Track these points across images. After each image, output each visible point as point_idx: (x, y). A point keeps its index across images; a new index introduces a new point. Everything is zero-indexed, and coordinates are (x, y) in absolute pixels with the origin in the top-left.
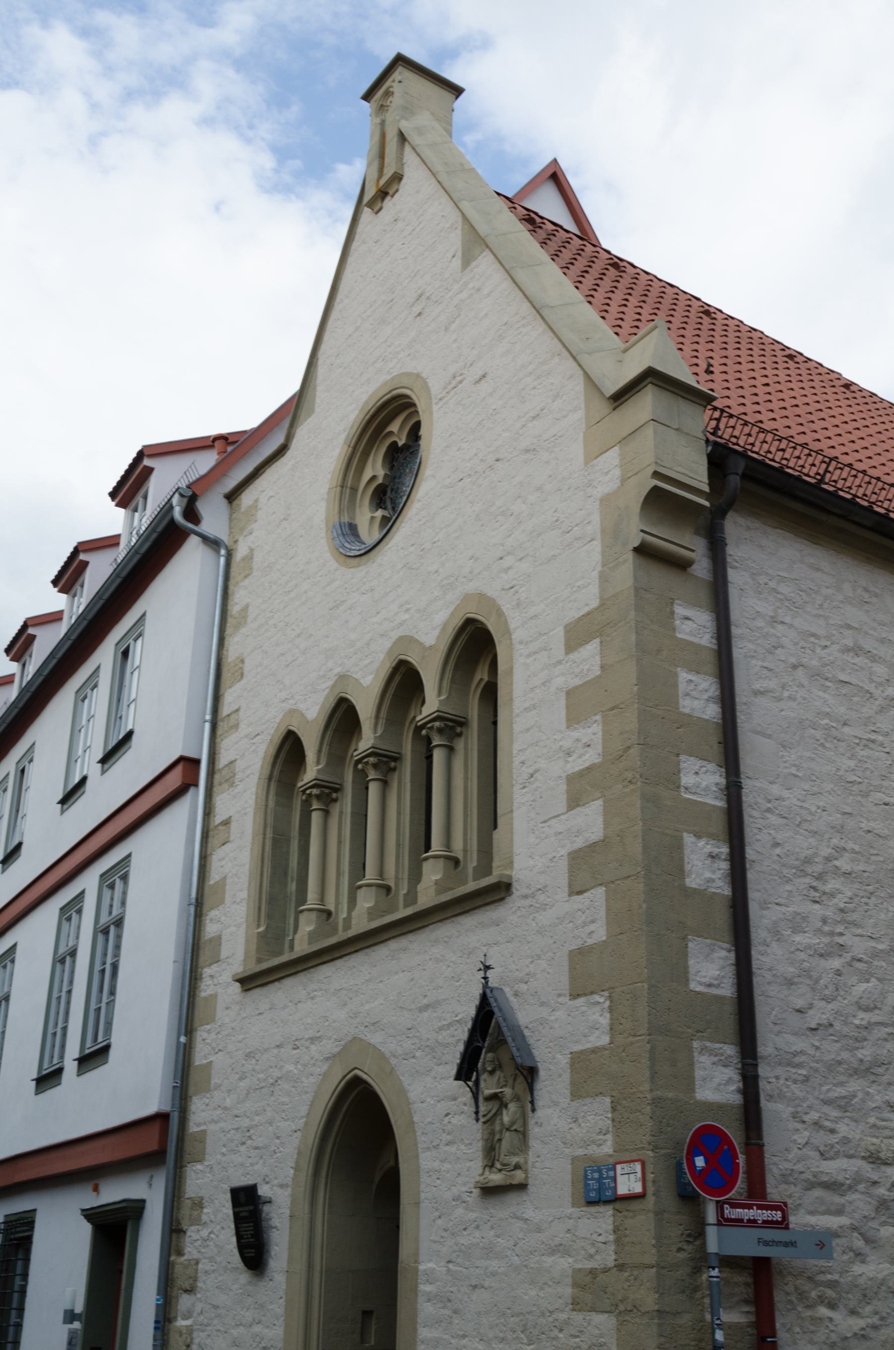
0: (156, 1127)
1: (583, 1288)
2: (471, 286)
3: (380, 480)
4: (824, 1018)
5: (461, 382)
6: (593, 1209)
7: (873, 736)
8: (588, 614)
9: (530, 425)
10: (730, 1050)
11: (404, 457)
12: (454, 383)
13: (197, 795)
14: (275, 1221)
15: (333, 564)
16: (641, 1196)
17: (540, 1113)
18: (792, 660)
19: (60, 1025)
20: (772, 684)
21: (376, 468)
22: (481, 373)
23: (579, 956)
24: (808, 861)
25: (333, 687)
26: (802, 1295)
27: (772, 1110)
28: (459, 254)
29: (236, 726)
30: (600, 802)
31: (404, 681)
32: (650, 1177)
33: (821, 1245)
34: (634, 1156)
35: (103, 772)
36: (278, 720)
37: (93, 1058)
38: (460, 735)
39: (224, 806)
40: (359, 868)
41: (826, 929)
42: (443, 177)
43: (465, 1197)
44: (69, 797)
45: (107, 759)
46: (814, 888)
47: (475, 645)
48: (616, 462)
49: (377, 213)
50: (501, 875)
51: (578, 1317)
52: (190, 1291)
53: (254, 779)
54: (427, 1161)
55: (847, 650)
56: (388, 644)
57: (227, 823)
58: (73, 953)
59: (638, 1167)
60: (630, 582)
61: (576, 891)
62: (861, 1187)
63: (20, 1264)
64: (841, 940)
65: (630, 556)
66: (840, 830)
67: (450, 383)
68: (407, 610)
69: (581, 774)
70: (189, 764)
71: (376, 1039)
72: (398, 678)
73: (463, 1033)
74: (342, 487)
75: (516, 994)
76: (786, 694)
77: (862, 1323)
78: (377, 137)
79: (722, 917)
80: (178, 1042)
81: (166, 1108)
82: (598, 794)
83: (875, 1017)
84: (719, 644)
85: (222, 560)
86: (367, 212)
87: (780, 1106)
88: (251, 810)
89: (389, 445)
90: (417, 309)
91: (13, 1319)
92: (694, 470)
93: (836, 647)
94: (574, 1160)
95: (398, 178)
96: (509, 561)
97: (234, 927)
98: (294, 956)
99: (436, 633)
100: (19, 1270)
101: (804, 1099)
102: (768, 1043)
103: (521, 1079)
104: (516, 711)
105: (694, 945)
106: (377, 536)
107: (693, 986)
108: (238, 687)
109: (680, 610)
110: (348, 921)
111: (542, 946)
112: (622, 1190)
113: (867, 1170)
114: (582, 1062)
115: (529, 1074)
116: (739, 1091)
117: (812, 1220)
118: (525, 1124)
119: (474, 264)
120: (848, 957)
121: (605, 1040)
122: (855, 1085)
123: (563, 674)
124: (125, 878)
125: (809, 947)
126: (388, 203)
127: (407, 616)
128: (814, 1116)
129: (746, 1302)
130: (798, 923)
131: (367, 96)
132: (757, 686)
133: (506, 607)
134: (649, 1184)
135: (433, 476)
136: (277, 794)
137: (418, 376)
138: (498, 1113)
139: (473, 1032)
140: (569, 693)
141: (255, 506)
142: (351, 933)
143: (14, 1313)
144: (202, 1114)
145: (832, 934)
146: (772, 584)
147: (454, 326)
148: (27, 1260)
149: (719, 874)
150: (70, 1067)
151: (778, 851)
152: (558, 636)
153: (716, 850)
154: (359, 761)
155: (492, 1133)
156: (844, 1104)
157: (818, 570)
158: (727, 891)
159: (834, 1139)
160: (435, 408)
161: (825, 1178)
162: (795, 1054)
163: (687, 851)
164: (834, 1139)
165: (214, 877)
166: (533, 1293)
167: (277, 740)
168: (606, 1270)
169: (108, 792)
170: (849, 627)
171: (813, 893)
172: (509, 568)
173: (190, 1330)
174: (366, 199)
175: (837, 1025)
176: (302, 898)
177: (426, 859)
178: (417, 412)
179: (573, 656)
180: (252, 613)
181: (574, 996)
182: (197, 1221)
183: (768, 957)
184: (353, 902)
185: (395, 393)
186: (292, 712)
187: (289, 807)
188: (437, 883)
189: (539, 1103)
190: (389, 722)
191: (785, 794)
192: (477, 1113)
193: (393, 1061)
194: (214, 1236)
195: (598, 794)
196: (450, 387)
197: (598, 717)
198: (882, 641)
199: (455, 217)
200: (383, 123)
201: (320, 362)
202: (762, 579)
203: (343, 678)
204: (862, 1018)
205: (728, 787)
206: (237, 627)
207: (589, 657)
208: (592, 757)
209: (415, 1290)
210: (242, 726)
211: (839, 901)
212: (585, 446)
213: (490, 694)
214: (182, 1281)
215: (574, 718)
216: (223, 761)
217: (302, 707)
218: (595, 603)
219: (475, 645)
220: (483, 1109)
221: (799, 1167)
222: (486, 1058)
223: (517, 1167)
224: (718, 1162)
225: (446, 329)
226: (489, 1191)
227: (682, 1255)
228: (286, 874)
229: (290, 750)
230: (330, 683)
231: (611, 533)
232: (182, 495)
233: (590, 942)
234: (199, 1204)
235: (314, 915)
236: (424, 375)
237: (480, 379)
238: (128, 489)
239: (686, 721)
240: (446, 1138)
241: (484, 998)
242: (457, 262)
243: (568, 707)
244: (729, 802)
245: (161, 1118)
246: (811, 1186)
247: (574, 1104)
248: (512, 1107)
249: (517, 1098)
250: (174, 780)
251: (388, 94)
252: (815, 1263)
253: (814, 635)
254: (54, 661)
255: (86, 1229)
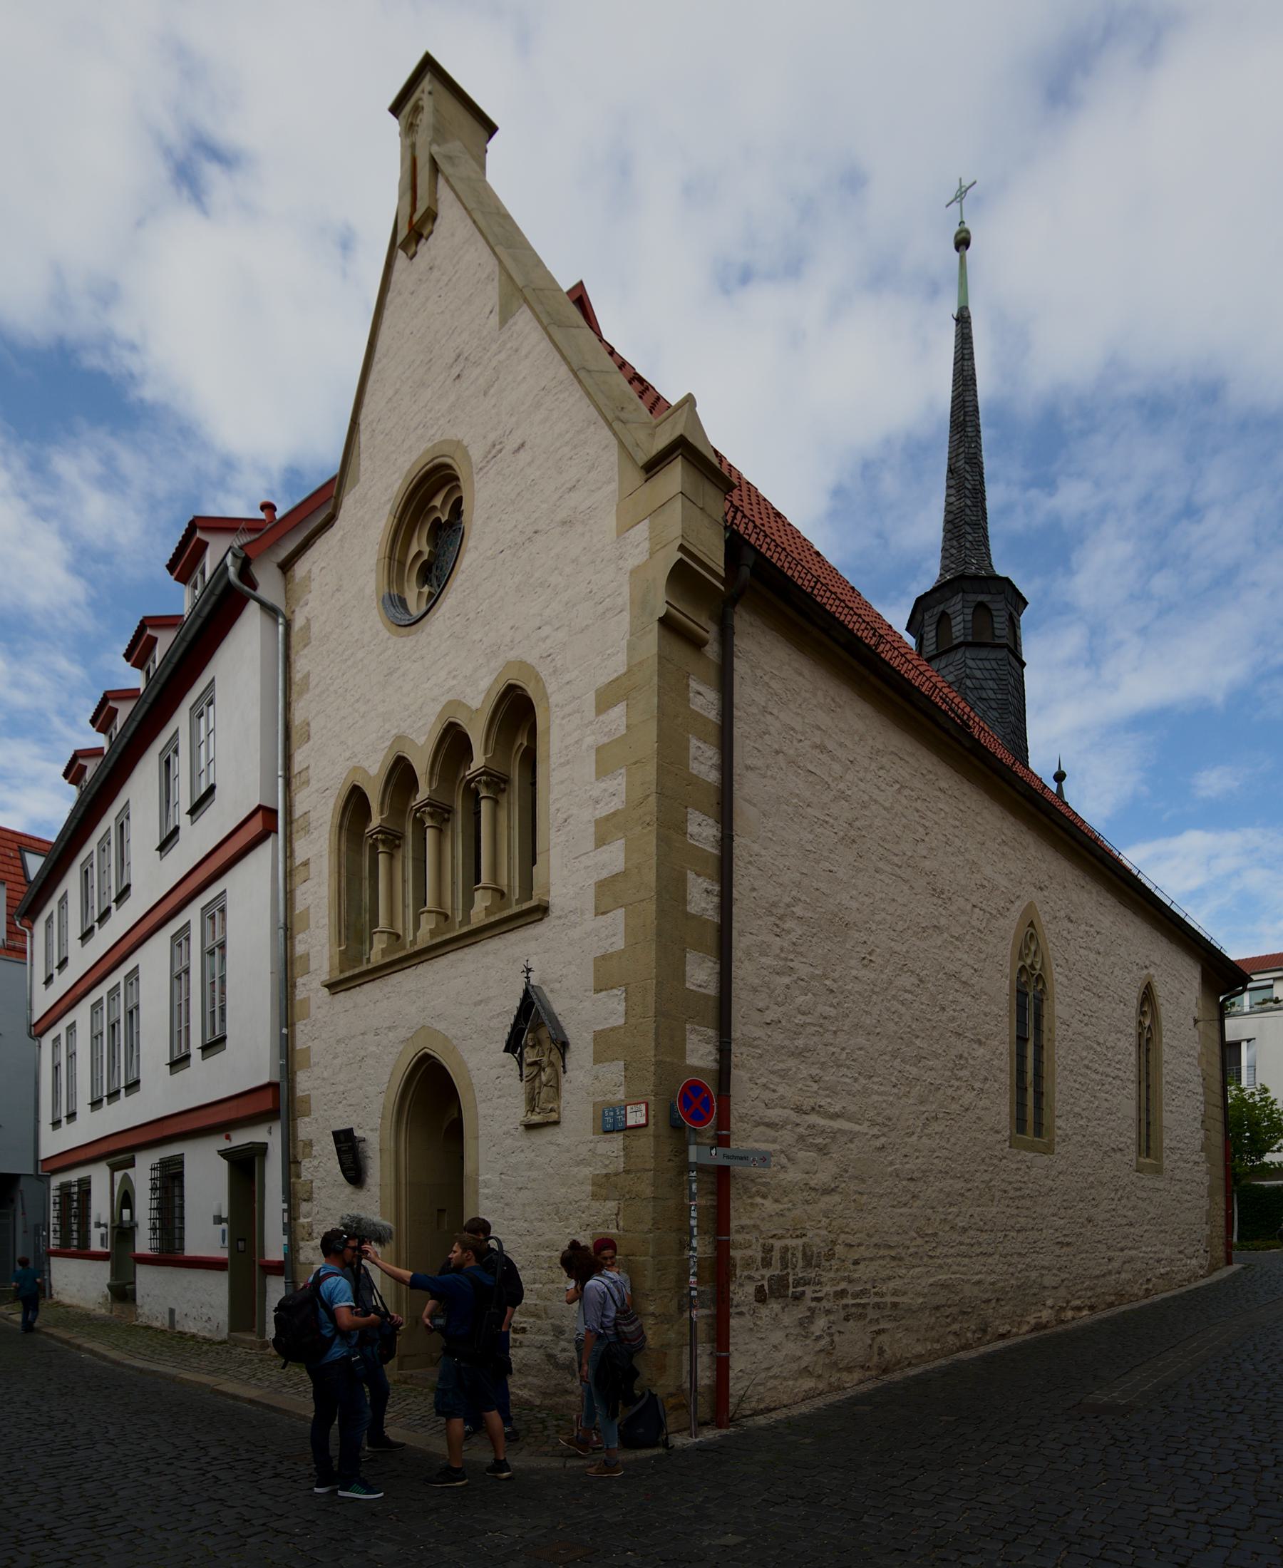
0: (270, 1092)
1: (600, 1186)
2: (509, 345)
3: (425, 557)
4: (775, 1017)
5: (500, 451)
6: (608, 1136)
7: (827, 819)
8: (617, 679)
9: (566, 496)
10: (711, 1033)
11: (448, 534)
12: (494, 452)
13: (277, 840)
14: (370, 1154)
15: (385, 633)
16: (646, 1125)
17: (568, 1074)
18: (776, 746)
19: (183, 1025)
20: (759, 763)
21: (420, 544)
22: (519, 441)
23: (602, 961)
24: (774, 904)
25: (391, 747)
26: (746, 1190)
27: (738, 1075)
28: (497, 309)
29: (307, 782)
30: (623, 841)
31: (453, 742)
32: (652, 1113)
33: (764, 1159)
34: (641, 1099)
35: (193, 823)
36: (344, 776)
37: (214, 1045)
38: (504, 790)
39: (303, 849)
40: (421, 900)
41: (783, 955)
42: (477, 216)
43: (513, 1132)
44: (166, 843)
45: (195, 810)
46: (777, 926)
47: (516, 710)
48: (646, 534)
49: (412, 258)
50: (540, 900)
51: (596, 1204)
52: (308, 1200)
53: (327, 827)
54: (483, 1109)
55: (815, 747)
56: (439, 708)
57: (306, 864)
58: (187, 971)
59: (643, 1107)
60: (655, 650)
61: (600, 912)
62: (789, 1127)
63: (177, 1190)
64: (791, 964)
65: (655, 626)
66: (798, 885)
67: (489, 452)
68: (454, 677)
69: (608, 818)
70: (266, 813)
71: (440, 1026)
72: (448, 740)
73: (510, 1020)
74: (390, 558)
75: (552, 991)
76: (769, 773)
77: (781, 1207)
78: (408, 163)
79: (711, 938)
80: (282, 1034)
81: (276, 1079)
82: (621, 835)
83: (808, 1019)
84: (723, 721)
85: (281, 628)
86: (401, 254)
87: (742, 1073)
88: (326, 853)
89: (433, 516)
90: (455, 371)
91: (177, 1224)
92: (714, 553)
93: (807, 742)
94: (595, 1104)
95: (431, 215)
96: (546, 630)
97: (319, 946)
98: (370, 966)
99: (483, 696)
100: (177, 1215)
101: (758, 1069)
102: (739, 1030)
103: (555, 1051)
104: (553, 766)
105: (691, 956)
106: (424, 608)
107: (688, 985)
108: (306, 747)
109: (694, 685)
110: (414, 942)
111: (580, 946)
112: (630, 1122)
113: (794, 1116)
114: (599, 1037)
115: (563, 1046)
116: (716, 1060)
117: (757, 1145)
118: (558, 1082)
119: (511, 322)
120: (795, 976)
121: (622, 1021)
122: (791, 1063)
123: (593, 733)
124: (223, 910)
125: (770, 967)
126: (423, 247)
127: (455, 682)
128: (764, 1080)
129: (712, 1193)
130: (764, 950)
131: (396, 109)
132: (749, 762)
133: (544, 672)
134: (651, 1118)
135: (476, 548)
136: (348, 841)
137: (459, 442)
138: (538, 1074)
139: (517, 1018)
140: (598, 750)
141: (308, 578)
142: (416, 948)
143: (177, 1221)
144: (304, 1083)
145: (786, 959)
146: (766, 678)
147: (492, 391)
148: (182, 1187)
149: (711, 906)
150: (196, 1054)
151: (754, 894)
152: (590, 698)
153: (710, 888)
154: (418, 810)
155: (533, 1088)
156: (783, 1074)
157: (801, 674)
158: (717, 919)
159: (774, 1096)
160: (476, 478)
161: (767, 1120)
162: (755, 1039)
163: (689, 885)
164: (774, 1096)
165: (299, 908)
166: (563, 1190)
167: (345, 793)
168: (617, 1174)
169: (199, 838)
170: (819, 728)
171: (775, 929)
172: (547, 637)
173: (310, 1225)
174: (400, 239)
175: (784, 1023)
176: (374, 921)
177: (477, 889)
178: (458, 487)
179: (603, 717)
180: (313, 680)
181: (597, 991)
182: (310, 1155)
183: (742, 971)
184: (417, 926)
185: (436, 461)
186: (356, 769)
187: (359, 852)
188: (486, 908)
189: (568, 1067)
190: (442, 779)
191: (763, 852)
192: (521, 1075)
193: (455, 1042)
194: (323, 1165)
195: (621, 835)
196: (490, 456)
197: (623, 771)
198: (841, 744)
199: (492, 264)
200: (413, 146)
201: (362, 427)
202: (759, 673)
203: (399, 738)
204: (800, 1019)
205: (722, 839)
206: (301, 694)
207: (617, 716)
208: (617, 804)
209: (476, 1193)
210: (312, 782)
211: (793, 937)
212: (618, 519)
213: (530, 760)
214: (301, 1191)
215: (603, 771)
216: (298, 811)
217: (365, 764)
218: (623, 670)
219: (516, 710)
220: (525, 1072)
221: (751, 1112)
222: (528, 1037)
223: (552, 1110)
224: (698, 1106)
225: (485, 394)
226: (530, 1127)
227: (671, 1164)
228: (360, 907)
229: (355, 801)
230: (388, 743)
231: (640, 604)
232: (234, 555)
233: (611, 950)
234: (309, 1144)
235: (385, 936)
236: (465, 443)
237: (519, 449)
238: (184, 562)
239: (693, 781)
240: (497, 1093)
241: (526, 992)
242: (495, 319)
243: (597, 762)
244: (722, 851)
245: (272, 1086)
246: (758, 1124)
247: (597, 1066)
248: (548, 1070)
249: (551, 1064)
250: (256, 826)
251: (417, 109)
252: (754, 1171)
253: (793, 729)
254: (134, 725)
255: (224, 1164)
